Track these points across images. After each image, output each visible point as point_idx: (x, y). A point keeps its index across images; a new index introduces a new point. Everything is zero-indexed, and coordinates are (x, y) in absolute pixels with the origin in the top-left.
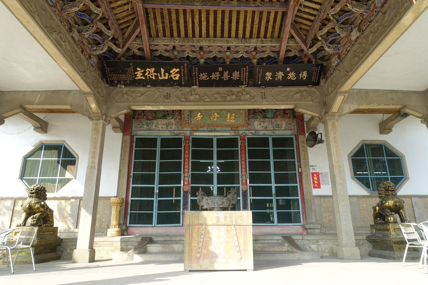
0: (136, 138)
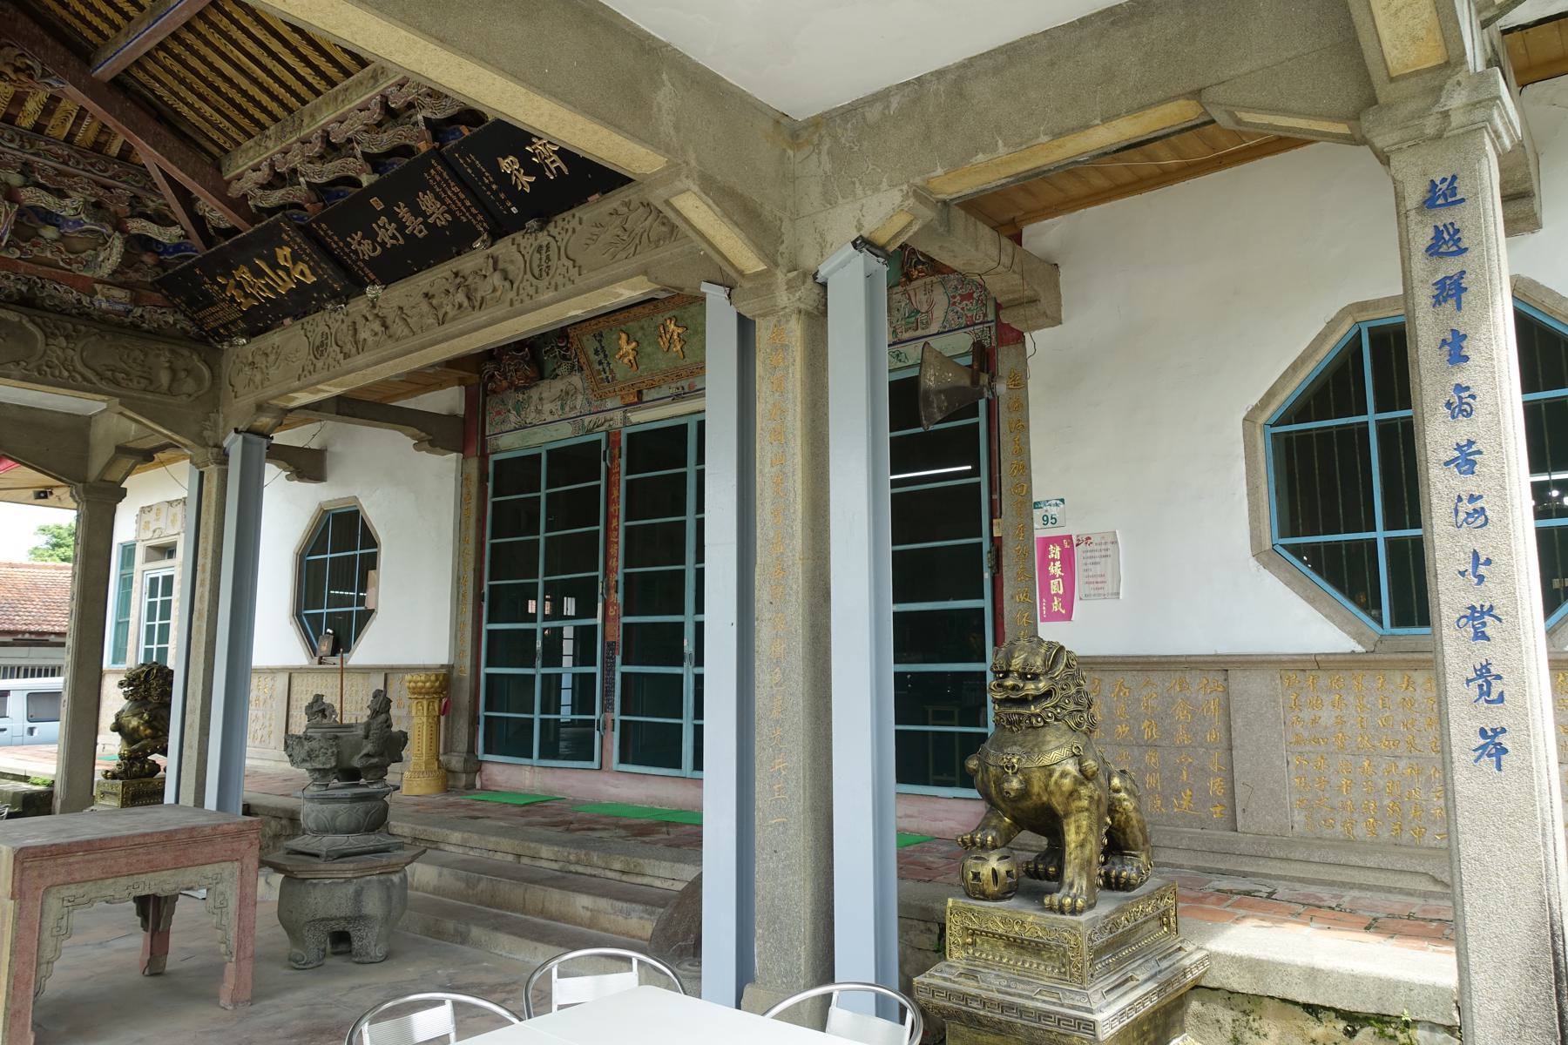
0: (496, 462)
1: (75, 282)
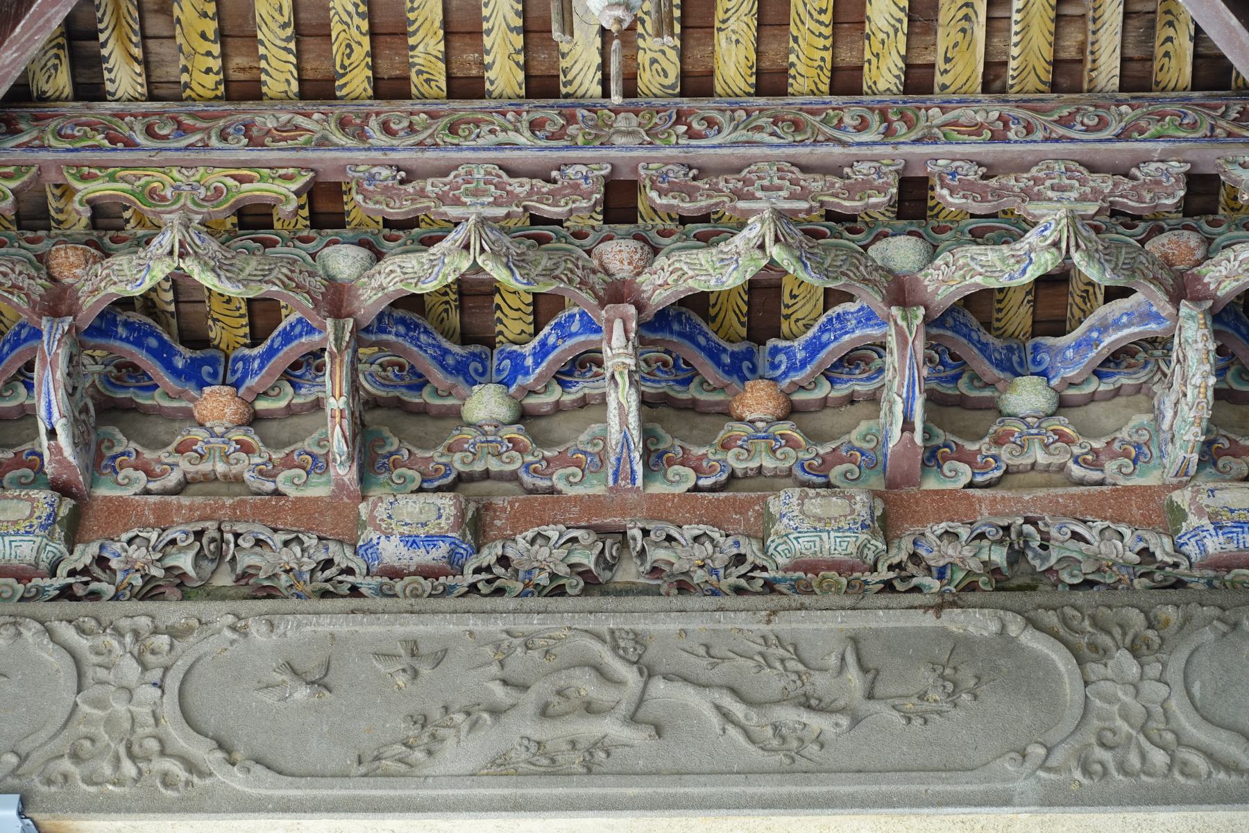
1: (1117, 505)
